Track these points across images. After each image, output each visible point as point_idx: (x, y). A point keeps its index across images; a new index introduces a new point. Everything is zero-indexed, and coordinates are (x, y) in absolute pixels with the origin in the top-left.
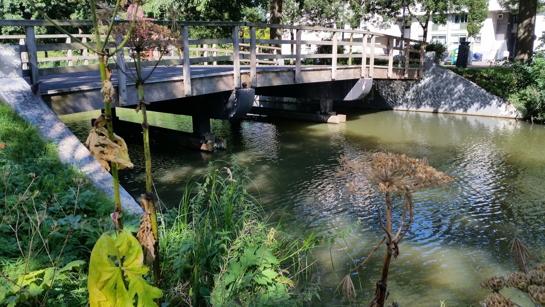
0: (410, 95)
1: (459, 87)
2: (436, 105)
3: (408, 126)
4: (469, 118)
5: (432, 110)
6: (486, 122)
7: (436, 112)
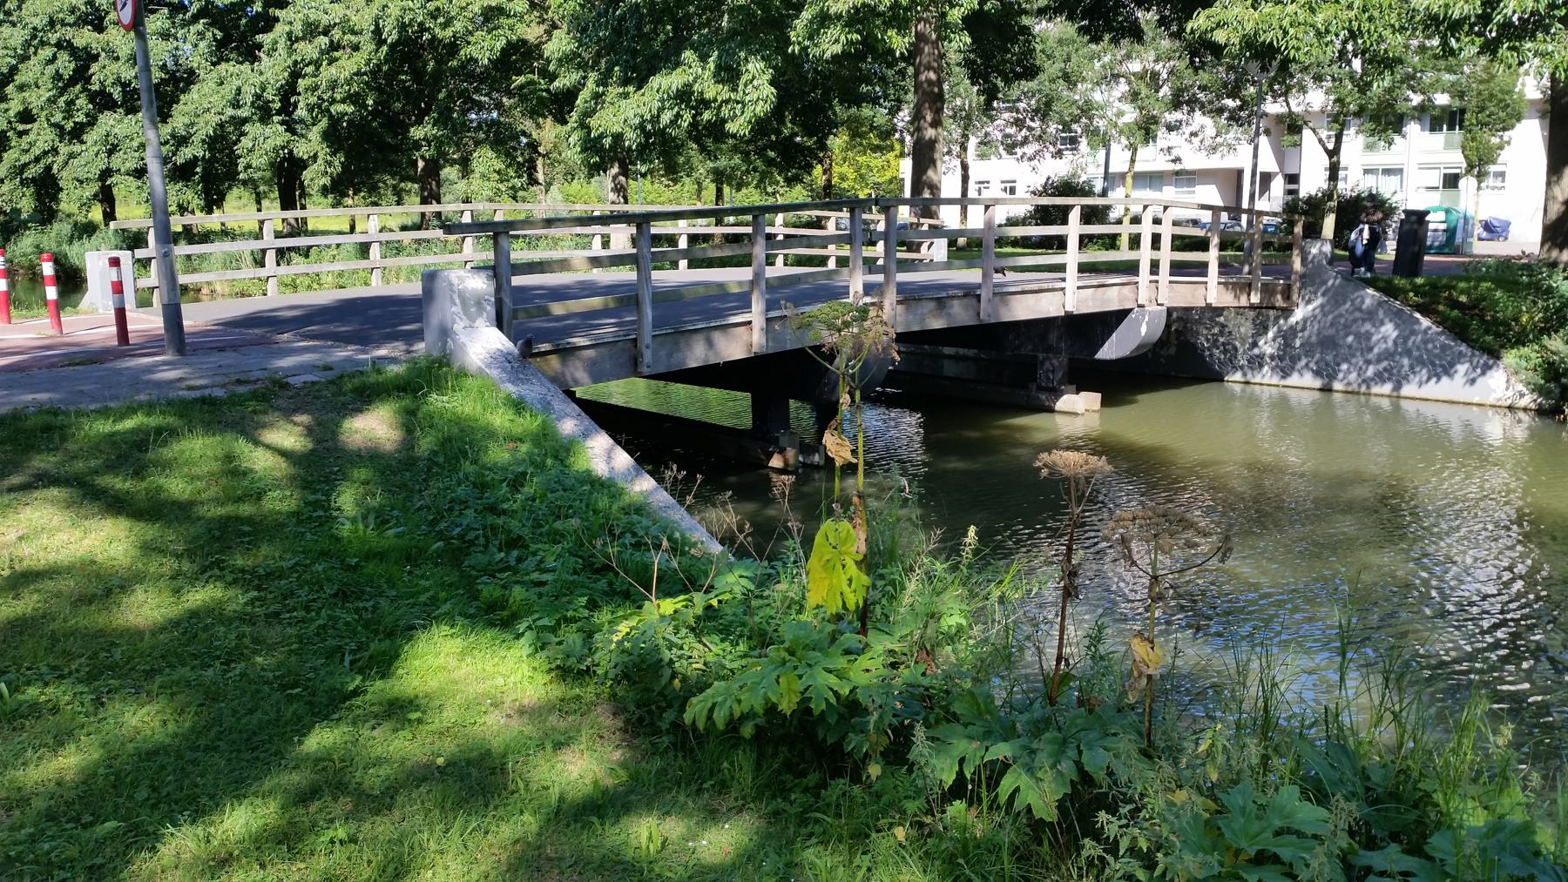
0: (1267, 346)
1: (1383, 329)
2: (1327, 373)
3: (1264, 423)
4: (1405, 404)
5: (1318, 383)
6: (1444, 415)
7: (1327, 389)
